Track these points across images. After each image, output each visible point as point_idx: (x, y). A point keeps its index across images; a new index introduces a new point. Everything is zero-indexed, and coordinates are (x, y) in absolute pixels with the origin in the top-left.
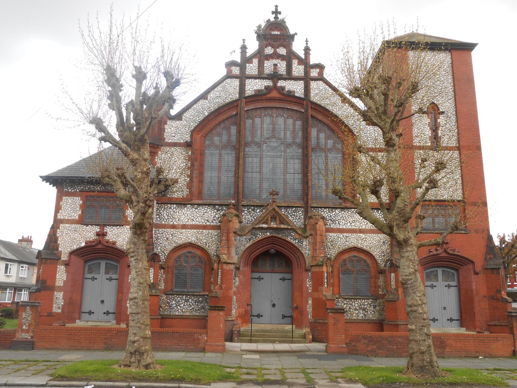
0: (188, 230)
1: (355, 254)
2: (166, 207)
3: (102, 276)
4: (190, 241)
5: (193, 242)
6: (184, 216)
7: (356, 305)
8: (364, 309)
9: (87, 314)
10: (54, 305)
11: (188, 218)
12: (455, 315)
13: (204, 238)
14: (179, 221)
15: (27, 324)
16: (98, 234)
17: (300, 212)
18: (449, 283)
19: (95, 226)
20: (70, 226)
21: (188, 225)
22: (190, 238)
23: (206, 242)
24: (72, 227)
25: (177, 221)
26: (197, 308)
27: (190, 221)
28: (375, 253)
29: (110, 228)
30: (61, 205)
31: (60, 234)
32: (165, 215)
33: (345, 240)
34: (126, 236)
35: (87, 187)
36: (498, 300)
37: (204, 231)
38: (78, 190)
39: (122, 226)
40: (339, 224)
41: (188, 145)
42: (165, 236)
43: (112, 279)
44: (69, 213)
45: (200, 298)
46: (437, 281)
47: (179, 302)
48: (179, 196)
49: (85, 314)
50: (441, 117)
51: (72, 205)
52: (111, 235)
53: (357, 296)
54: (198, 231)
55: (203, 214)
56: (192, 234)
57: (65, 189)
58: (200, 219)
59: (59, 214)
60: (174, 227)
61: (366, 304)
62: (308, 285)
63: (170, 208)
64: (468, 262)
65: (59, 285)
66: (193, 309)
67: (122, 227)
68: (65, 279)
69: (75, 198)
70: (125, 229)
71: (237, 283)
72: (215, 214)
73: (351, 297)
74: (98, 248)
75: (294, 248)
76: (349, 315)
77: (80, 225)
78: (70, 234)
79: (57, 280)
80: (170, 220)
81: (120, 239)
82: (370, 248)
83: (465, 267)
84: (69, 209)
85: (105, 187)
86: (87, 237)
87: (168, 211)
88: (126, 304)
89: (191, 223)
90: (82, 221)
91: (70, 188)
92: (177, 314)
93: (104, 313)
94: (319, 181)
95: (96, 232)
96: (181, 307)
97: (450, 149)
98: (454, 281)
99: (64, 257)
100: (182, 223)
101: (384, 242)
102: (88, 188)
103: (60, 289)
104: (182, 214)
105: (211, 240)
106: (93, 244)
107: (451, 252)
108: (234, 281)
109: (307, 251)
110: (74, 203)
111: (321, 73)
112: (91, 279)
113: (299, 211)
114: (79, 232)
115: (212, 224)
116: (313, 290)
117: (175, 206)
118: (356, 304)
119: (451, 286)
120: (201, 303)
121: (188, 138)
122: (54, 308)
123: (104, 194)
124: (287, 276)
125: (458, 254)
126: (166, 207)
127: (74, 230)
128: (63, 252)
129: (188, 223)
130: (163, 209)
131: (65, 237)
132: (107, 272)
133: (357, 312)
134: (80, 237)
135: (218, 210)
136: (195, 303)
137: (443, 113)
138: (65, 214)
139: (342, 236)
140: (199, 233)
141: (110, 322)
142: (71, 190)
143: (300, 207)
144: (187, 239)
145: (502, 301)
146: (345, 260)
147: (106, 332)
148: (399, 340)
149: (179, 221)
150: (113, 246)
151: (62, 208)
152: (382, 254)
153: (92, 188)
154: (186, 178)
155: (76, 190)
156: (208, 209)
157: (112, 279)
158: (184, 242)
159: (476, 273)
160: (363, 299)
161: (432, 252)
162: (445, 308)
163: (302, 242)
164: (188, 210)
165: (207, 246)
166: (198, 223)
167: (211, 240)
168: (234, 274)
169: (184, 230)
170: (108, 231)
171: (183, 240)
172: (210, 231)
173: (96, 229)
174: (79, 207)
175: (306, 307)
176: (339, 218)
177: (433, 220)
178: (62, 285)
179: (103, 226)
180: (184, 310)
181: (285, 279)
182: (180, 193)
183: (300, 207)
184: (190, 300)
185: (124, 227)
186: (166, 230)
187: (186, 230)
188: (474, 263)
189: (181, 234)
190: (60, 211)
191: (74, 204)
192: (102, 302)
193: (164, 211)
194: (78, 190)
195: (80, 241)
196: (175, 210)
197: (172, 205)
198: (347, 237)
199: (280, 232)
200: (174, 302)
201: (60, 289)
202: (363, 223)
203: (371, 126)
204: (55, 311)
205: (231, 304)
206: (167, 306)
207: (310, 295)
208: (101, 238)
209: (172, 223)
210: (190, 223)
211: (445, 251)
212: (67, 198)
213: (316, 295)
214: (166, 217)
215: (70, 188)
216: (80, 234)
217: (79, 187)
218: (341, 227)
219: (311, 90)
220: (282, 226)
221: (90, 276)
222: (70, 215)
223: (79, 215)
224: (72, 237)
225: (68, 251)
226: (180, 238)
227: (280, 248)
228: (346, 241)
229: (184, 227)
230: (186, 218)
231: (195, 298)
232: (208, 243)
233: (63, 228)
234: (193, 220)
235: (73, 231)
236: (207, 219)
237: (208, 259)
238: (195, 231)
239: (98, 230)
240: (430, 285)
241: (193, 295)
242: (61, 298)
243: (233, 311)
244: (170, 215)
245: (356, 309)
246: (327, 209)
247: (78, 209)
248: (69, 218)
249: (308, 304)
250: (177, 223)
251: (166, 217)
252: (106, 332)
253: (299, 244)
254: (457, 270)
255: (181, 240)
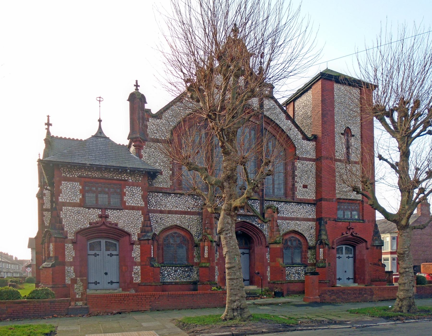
0: (174, 215)
1: (293, 235)
2: (154, 195)
3: (103, 252)
4: (175, 224)
5: (178, 224)
6: (169, 203)
7: (294, 271)
8: (298, 274)
9: (94, 284)
10: (66, 278)
11: (173, 205)
12: (351, 276)
13: (186, 221)
14: (165, 207)
15: (80, 294)
16: (100, 216)
17: (257, 204)
18: (96, 252)
19: (96, 209)
20: (73, 208)
21: (173, 211)
22: (176, 221)
23: (188, 225)
24: (75, 209)
25: (164, 207)
26: (184, 276)
27: (174, 207)
28: (306, 235)
29: (111, 211)
30: (61, 190)
31: (64, 216)
32: (153, 202)
33: (287, 225)
34: (126, 218)
35: (85, 173)
36: (379, 265)
37: (186, 216)
38: (76, 176)
39: (122, 210)
40: (283, 213)
41: (170, 142)
42: (154, 219)
43: (113, 255)
44: (70, 197)
45: (186, 268)
46: (342, 254)
47: (170, 272)
48: (164, 186)
49: (92, 284)
50: (353, 138)
51: (72, 190)
52: (113, 217)
53: (293, 265)
54: (182, 216)
55: (184, 202)
56: (176, 218)
57: (63, 174)
58: (182, 206)
59: (60, 198)
60: (161, 212)
61: (300, 269)
62: (267, 258)
63: (157, 196)
64: (362, 240)
65: (69, 260)
66: (181, 277)
67: (122, 211)
68: (74, 255)
69: (74, 183)
70: (125, 212)
71: (218, 257)
72: (194, 202)
73: (290, 265)
74: (102, 229)
75: (258, 230)
76: (289, 278)
77: (82, 208)
78: (74, 216)
79: (66, 256)
80: (158, 206)
81: (121, 221)
82: (303, 231)
83: (361, 245)
84: (70, 193)
85: (103, 175)
86: (90, 218)
87: (155, 199)
88: (132, 275)
89: (176, 209)
90: (83, 204)
91: (68, 174)
92: (169, 281)
93: (109, 283)
94: (268, 180)
95: (99, 215)
96: (171, 276)
97: (356, 163)
98: (351, 254)
99: (71, 237)
100: (168, 209)
101: (311, 228)
102: (86, 174)
103: (71, 264)
104: (168, 201)
105: (192, 223)
106: (98, 225)
107: (355, 235)
108: (216, 255)
109: (267, 233)
110: (74, 188)
111: (271, 92)
112: (94, 255)
113: (256, 203)
114: (82, 214)
115: (192, 210)
116: (271, 261)
117: (161, 194)
118: (294, 270)
119: (350, 257)
120: (187, 272)
121: (168, 136)
122: (66, 281)
123: (102, 181)
124: (246, 251)
125: (359, 236)
126: (154, 195)
127: (77, 212)
128: (68, 231)
129: (173, 209)
130: (151, 197)
131: (69, 218)
132: (107, 250)
133: (294, 275)
134: (84, 219)
135: (196, 199)
136: (183, 272)
137: (353, 136)
138: (66, 198)
139: (285, 222)
140: (183, 217)
141: (116, 289)
142: (70, 175)
143: (257, 200)
144: (173, 222)
145: (382, 266)
146: (286, 240)
147: (150, 296)
148: (349, 291)
149: (165, 207)
150: (115, 227)
151: (63, 192)
152: (310, 236)
153: (90, 174)
154: (169, 171)
155: (75, 176)
156: (188, 198)
157: (113, 255)
158: (171, 224)
159: (367, 249)
160: (298, 267)
161: (344, 234)
162: (346, 272)
163: (263, 226)
164: (173, 198)
165: (189, 228)
166: (181, 209)
167: (192, 223)
168: (216, 250)
169: (170, 215)
170: (110, 214)
171: (170, 223)
172: (191, 216)
173: (98, 212)
174: (79, 191)
175: (266, 273)
176: (284, 209)
177: (344, 213)
178: (71, 260)
179: (104, 209)
180: (174, 278)
181: (244, 253)
182: (165, 184)
183: (257, 200)
184: (179, 271)
185: (124, 210)
186: (155, 215)
187: (172, 215)
188: (367, 242)
189: (168, 218)
190: (61, 195)
191: (74, 189)
192: (106, 274)
193: (152, 199)
194: (76, 176)
195: (84, 222)
196: (161, 198)
197: (159, 194)
198: (288, 223)
199: (248, 218)
200: (166, 272)
201: (71, 264)
202: (299, 213)
203: (305, 141)
204: (68, 282)
205: (214, 272)
206: (161, 275)
207: (269, 264)
208: (104, 219)
209: (159, 209)
210: (175, 209)
211: (352, 234)
212: (66, 183)
213: (273, 264)
214: (155, 204)
215: (68, 174)
216: (83, 216)
217: (77, 173)
218: (285, 216)
219: (264, 106)
220: (249, 213)
221: (93, 252)
222: (71, 199)
223: (80, 198)
224: (76, 218)
225: (74, 231)
226: (167, 221)
227: (248, 231)
228: (288, 226)
229: (170, 212)
230: (171, 205)
231: (182, 269)
232: (190, 226)
233: (65, 210)
234: (177, 207)
235: (76, 213)
236: (188, 206)
237: (190, 238)
238: (179, 216)
239: (100, 213)
240: (93, 253)
241: (181, 266)
242: (72, 271)
243: (216, 277)
244: (157, 202)
245: (293, 274)
246: (276, 202)
247: (79, 193)
248: (70, 201)
249: (267, 270)
250: (164, 209)
251: (155, 204)
252: (150, 296)
253: (261, 227)
254: (354, 247)
255: (168, 223)
